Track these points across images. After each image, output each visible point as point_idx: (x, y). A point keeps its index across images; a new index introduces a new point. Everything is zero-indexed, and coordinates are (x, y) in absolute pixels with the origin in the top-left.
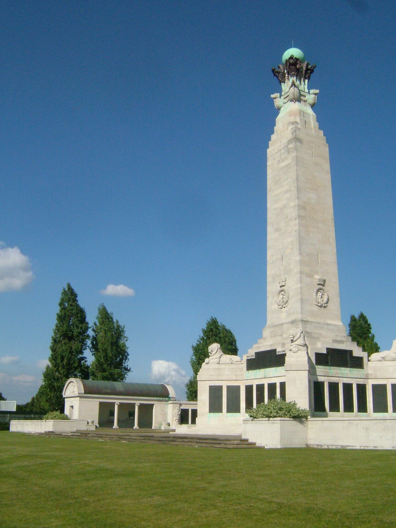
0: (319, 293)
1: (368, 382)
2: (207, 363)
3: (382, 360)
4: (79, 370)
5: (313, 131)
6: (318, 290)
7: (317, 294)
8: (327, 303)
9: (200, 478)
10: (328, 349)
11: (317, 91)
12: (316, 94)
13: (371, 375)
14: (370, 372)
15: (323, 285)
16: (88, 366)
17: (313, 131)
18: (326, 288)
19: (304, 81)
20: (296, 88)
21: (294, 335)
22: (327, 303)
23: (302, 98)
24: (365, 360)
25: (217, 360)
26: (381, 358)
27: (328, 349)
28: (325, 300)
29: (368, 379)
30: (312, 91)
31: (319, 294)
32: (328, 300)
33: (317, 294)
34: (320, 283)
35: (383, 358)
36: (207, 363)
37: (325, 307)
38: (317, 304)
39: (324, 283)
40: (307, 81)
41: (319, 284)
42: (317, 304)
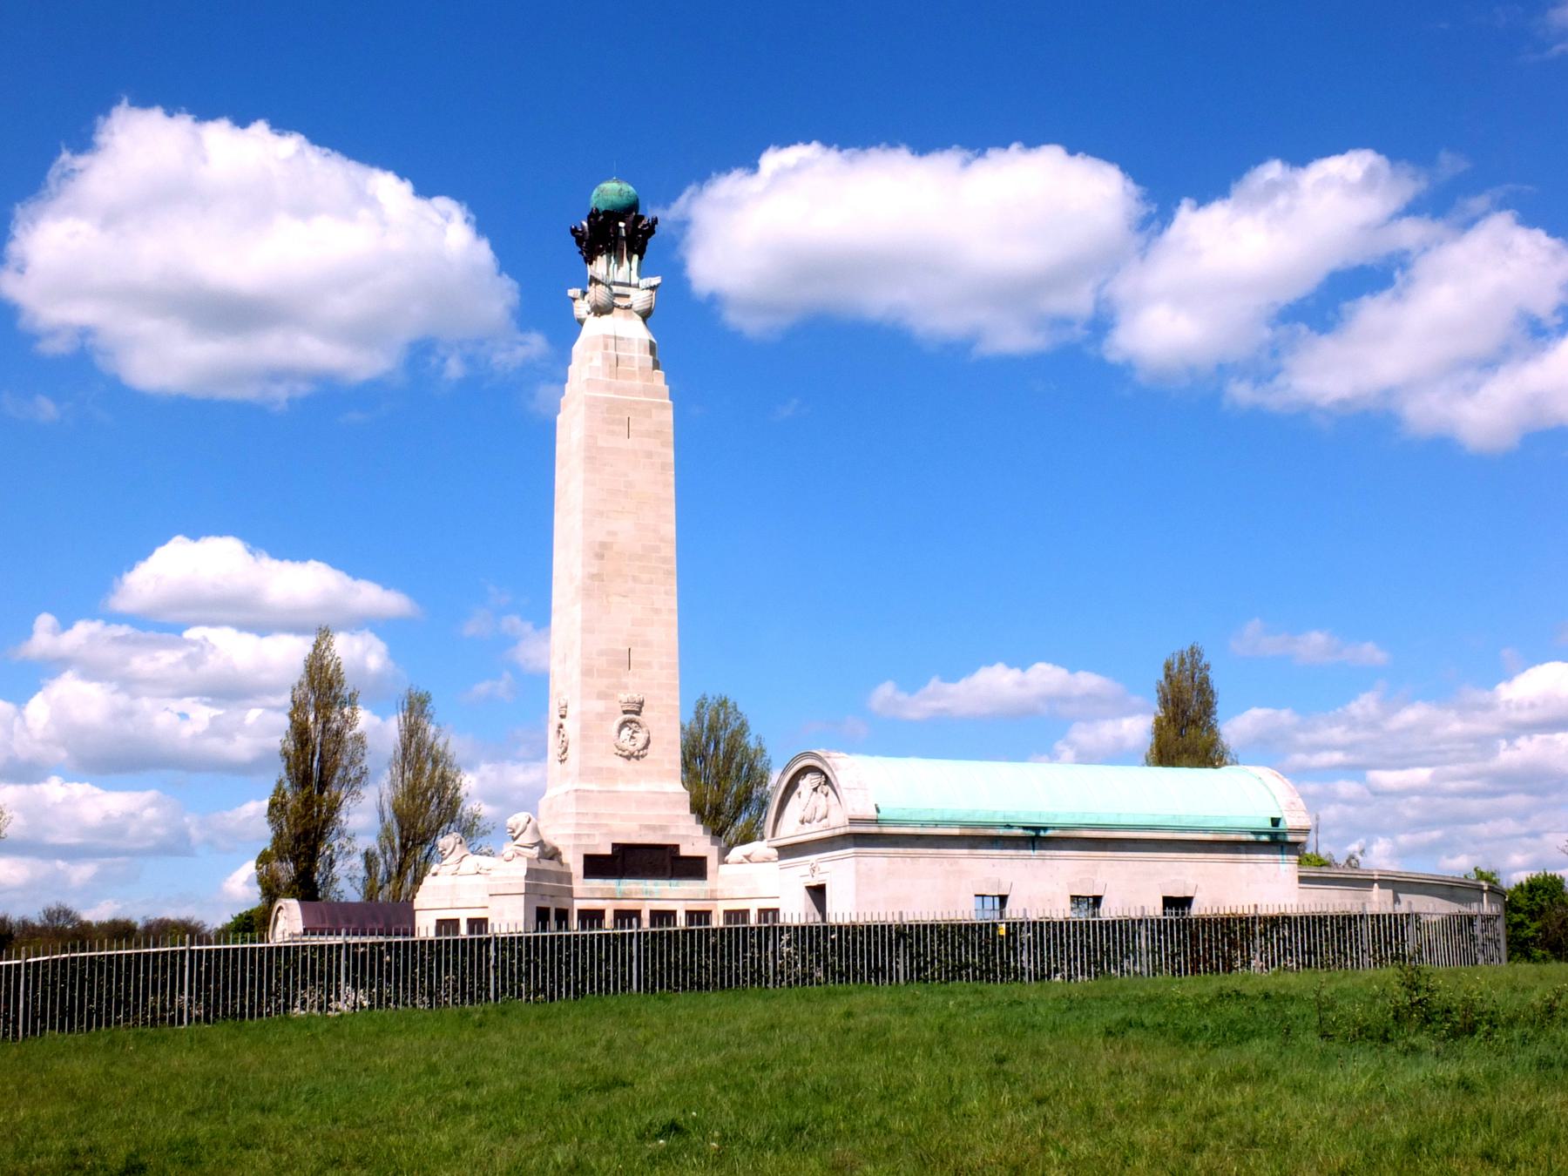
0: (627, 729)
1: (716, 905)
2: (435, 874)
3: (745, 860)
4: (444, 1146)
5: (617, 396)
6: (624, 724)
7: (619, 732)
8: (646, 747)
9: (188, 936)
10: (614, 845)
11: (656, 281)
12: (652, 288)
13: (722, 891)
14: (720, 885)
15: (638, 713)
16: (10, 931)
17: (617, 396)
18: (646, 716)
19: (630, 260)
20: (600, 286)
21: (514, 827)
22: (646, 747)
23: (618, 301)
24: (712, 864)
25: (454, 867)
26: (742, 858)
27: (614, 845)
28: (640, 745)
29: (717, 900)
30: (645, 283)
31: (626, 732)
32: (648, 741)
33: (619, 732)
34: (629, 708)
35: (747, 857)
36: (435, 874)
37: (637, 758)
38: (620, 752)
39: (640, 708)
40: (636, 258)
41: (625, 712)
42: (620, 752)
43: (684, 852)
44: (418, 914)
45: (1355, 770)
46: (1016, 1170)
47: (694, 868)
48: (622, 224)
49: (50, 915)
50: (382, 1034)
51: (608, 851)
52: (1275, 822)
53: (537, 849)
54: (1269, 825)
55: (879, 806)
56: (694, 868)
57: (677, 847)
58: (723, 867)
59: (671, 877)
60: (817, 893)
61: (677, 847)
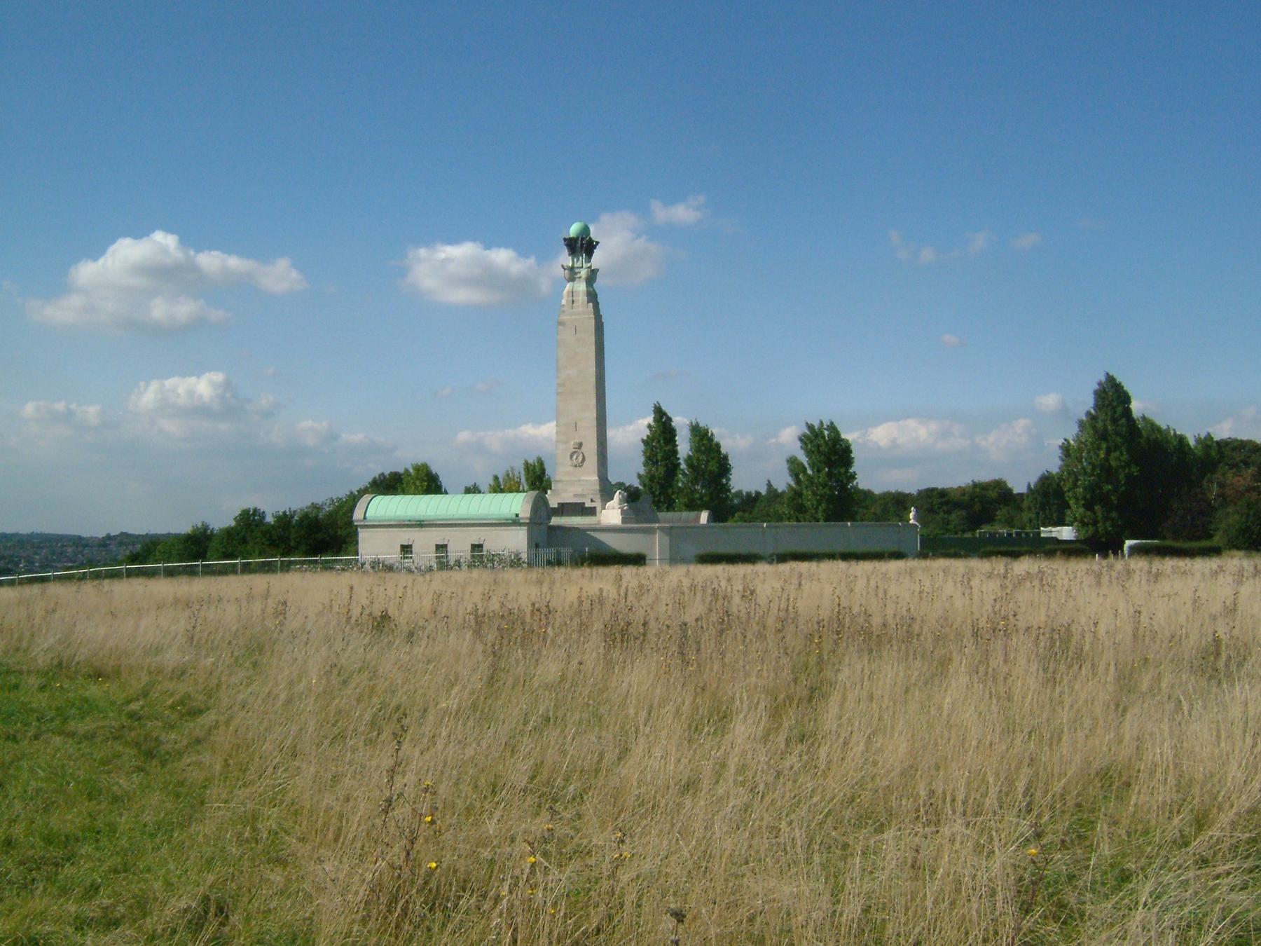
24: (598, 509)
43: (586, 506)
44: (363, 535)
45: (1060, 637)
46: (677, 942)
47: (592, 512)
48: (833, 459)
49: (196, 529)
50: (280, 607)
51: (556, 506)
52: (517, 515)
53: (517, 504)
54: (514, 516)
55: (470, 484)
56: (592, 512)
57: (584, 503)
58: (603, 511)
59: (582, 515)
60: (406, 549)
61: (584, 503)
